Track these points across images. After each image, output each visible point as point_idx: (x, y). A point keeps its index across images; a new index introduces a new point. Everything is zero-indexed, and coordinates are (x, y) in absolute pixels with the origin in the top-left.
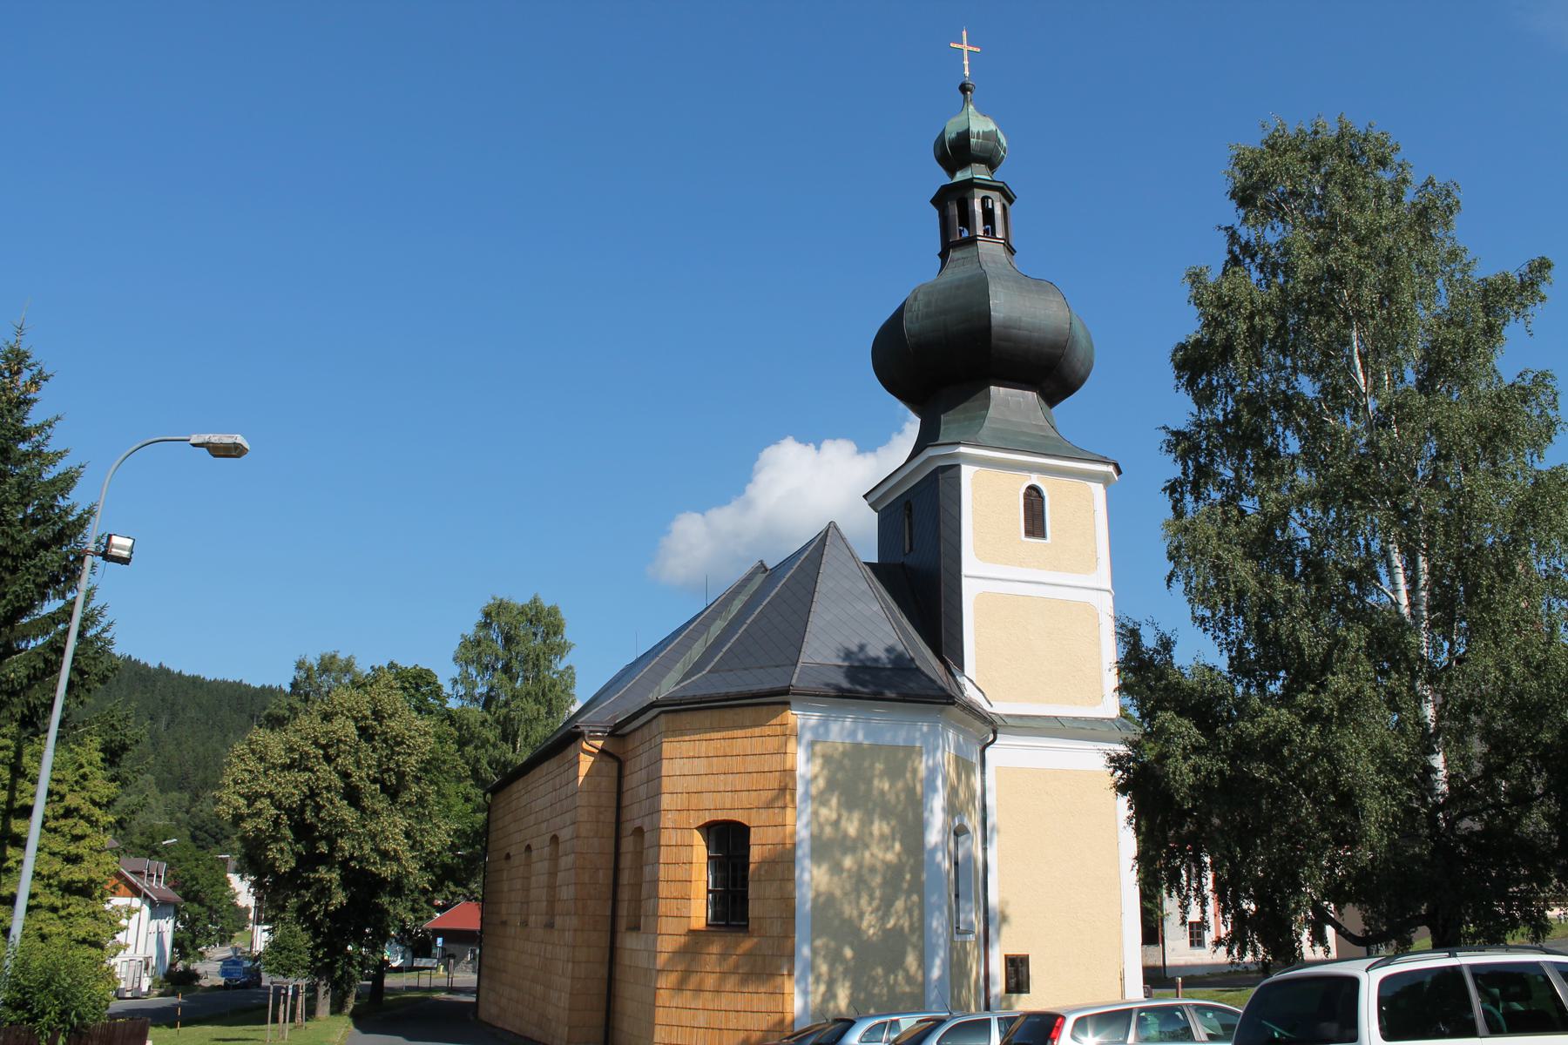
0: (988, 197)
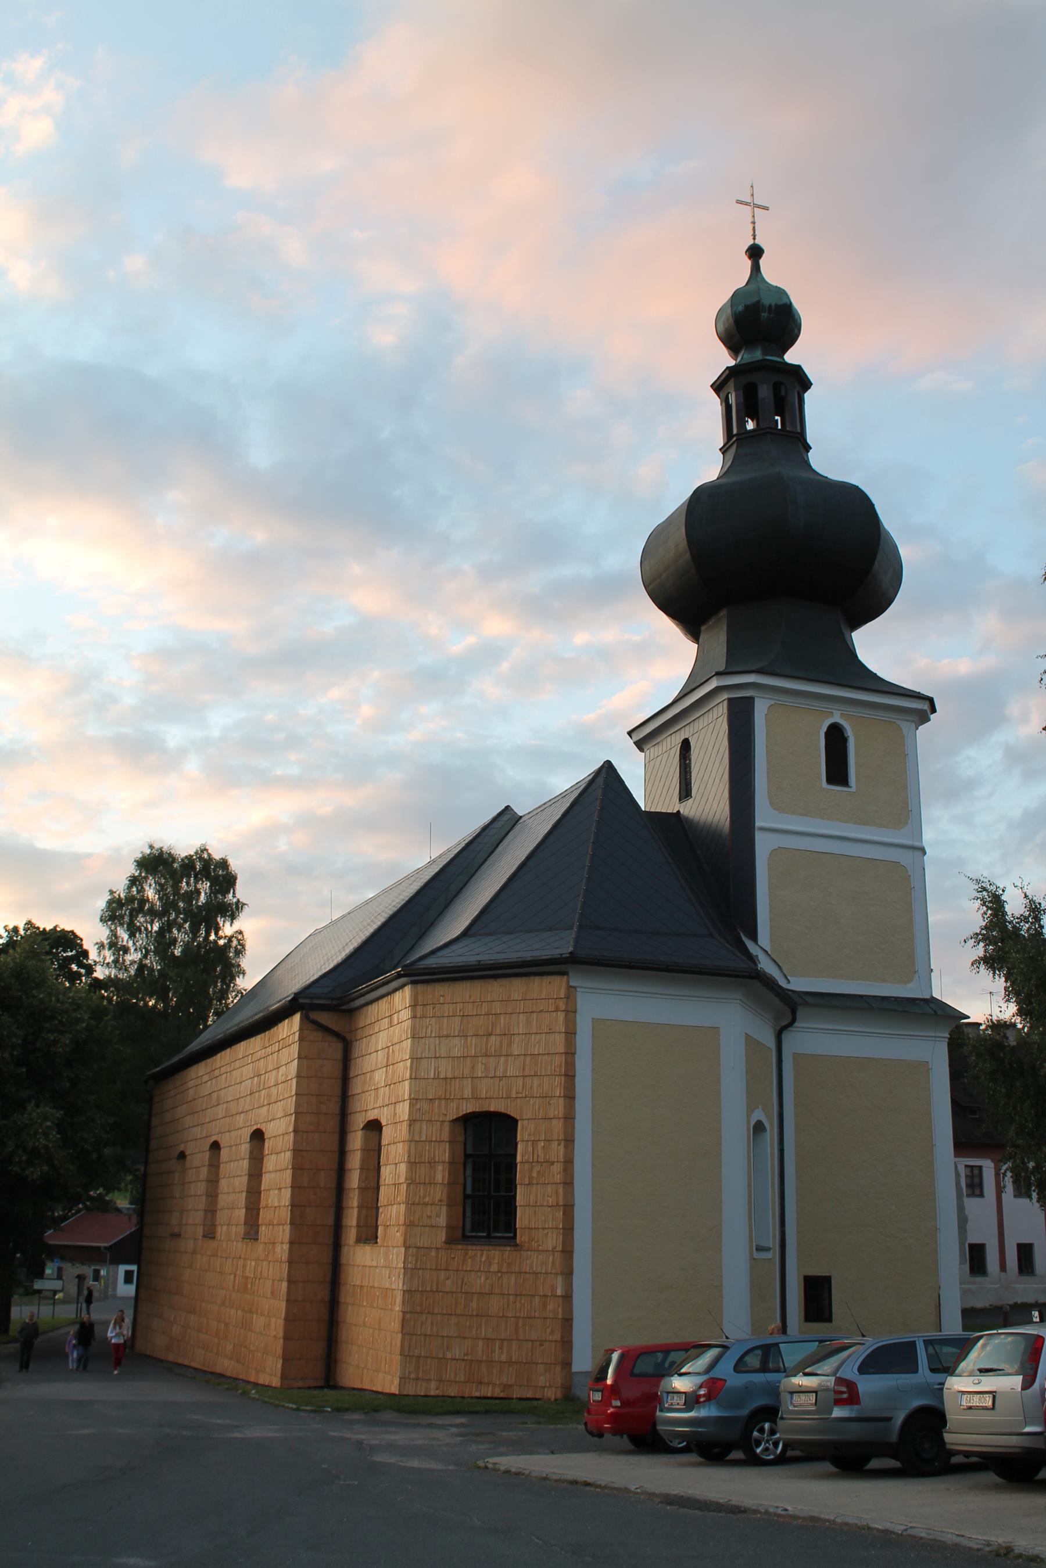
0: (781, 383)
